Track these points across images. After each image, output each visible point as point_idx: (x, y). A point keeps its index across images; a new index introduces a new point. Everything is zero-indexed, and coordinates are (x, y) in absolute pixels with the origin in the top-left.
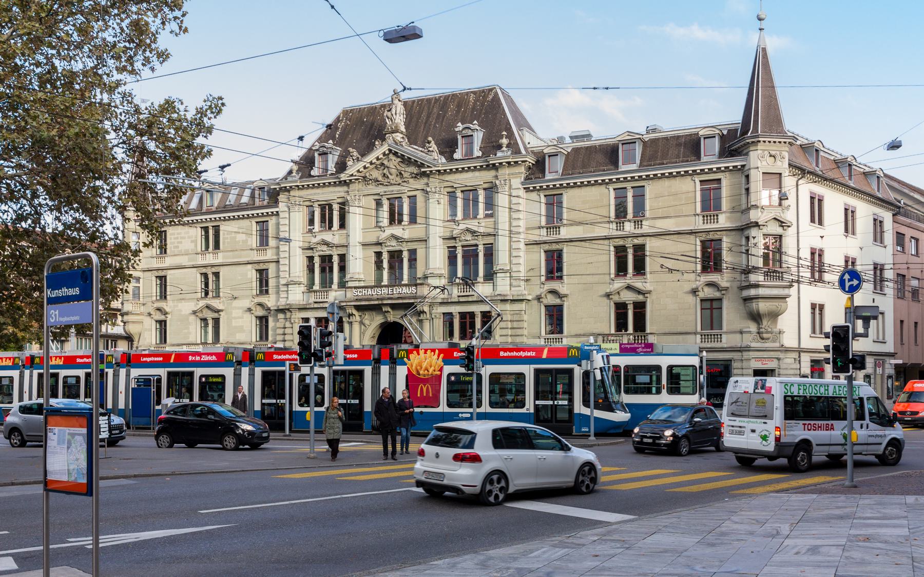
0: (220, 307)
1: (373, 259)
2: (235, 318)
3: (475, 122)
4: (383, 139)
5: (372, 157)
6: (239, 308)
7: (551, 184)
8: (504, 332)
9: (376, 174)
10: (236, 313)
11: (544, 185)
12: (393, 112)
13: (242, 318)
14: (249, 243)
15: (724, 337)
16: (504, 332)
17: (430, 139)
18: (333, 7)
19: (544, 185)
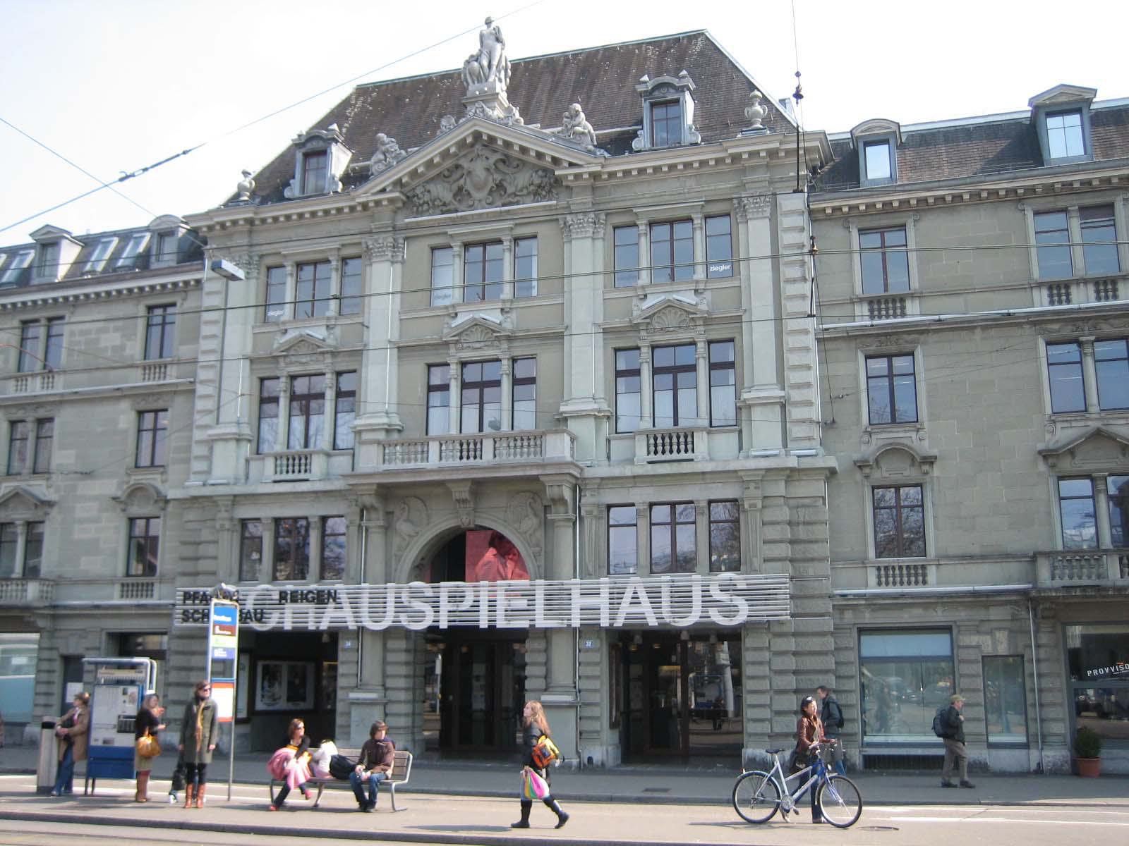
0: (51, 495)
1: (312, 441)
2: (81, 521)
3: (684, 72)
4: (460, 111)
5: (432, 151)
6: (96, 498)
7: (879, 201)
8: (772, 532)
9: (442, 191)
10: (81, 510)
11: (862, 203)
12: (485, 63)
13: (96, 520)
14: (128, 352)
15: (932, 573)
16: (772, 532)
17: (578, 107)
18: (184, 153)
19: (862, 203)
